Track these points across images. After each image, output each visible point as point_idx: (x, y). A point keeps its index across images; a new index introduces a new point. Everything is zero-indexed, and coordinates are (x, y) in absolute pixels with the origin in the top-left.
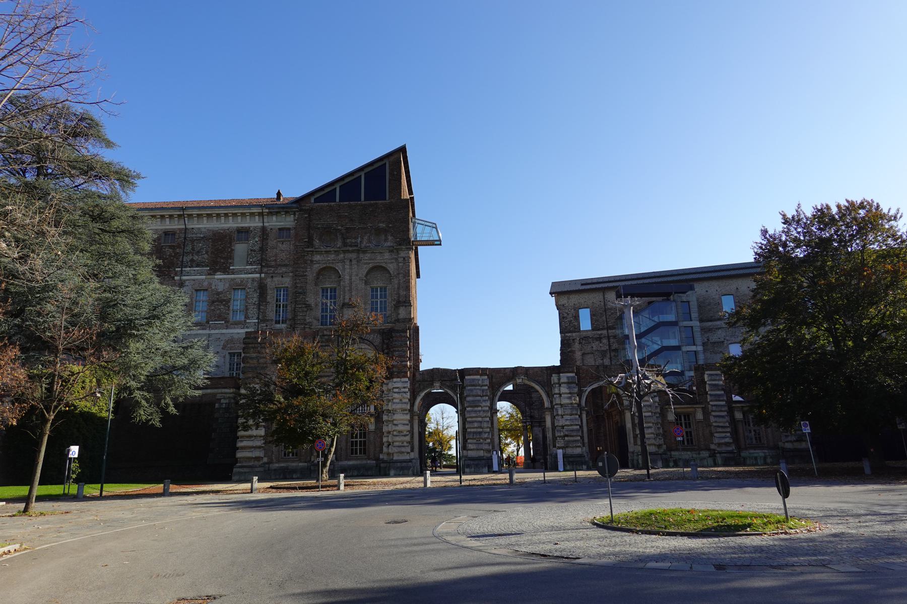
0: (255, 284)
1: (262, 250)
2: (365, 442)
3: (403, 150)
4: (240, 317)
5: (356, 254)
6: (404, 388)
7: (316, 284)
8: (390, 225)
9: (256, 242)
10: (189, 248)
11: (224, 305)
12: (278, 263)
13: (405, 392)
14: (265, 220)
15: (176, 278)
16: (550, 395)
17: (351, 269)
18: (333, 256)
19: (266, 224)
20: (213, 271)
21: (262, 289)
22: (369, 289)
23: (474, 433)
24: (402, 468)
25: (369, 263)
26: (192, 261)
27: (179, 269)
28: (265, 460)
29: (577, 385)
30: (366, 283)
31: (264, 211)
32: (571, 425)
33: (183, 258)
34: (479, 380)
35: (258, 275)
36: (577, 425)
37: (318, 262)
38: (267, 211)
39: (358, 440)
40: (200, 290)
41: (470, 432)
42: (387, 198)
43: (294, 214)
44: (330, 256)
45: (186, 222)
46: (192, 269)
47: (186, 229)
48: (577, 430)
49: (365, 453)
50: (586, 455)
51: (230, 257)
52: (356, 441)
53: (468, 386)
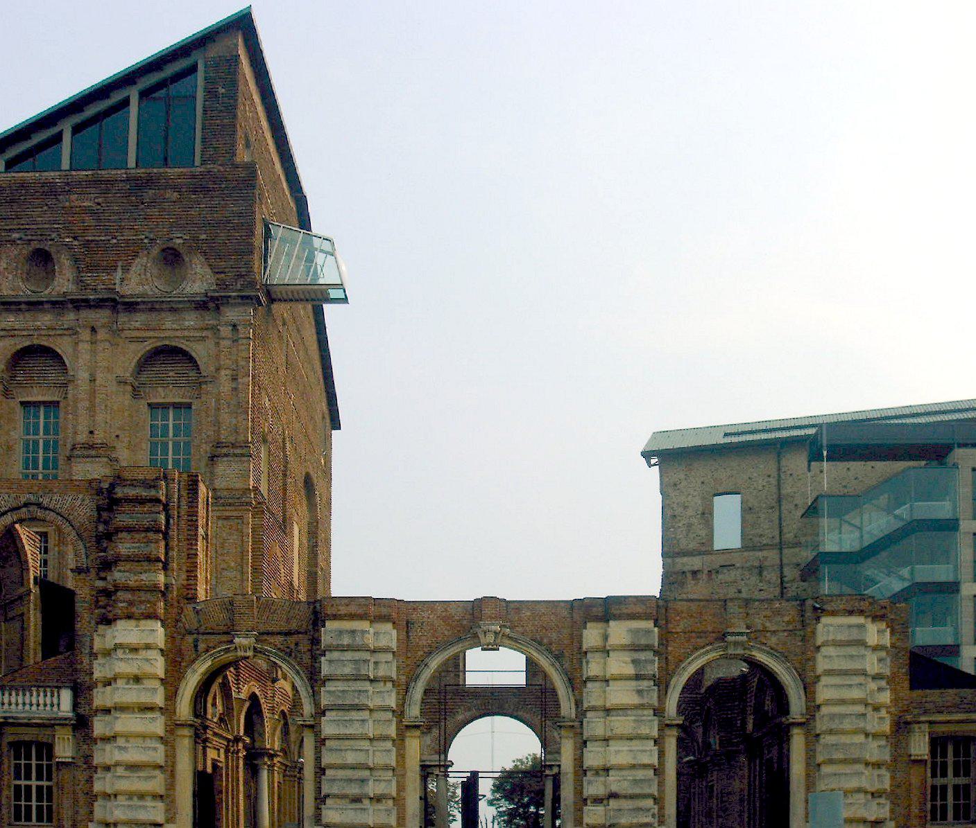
2: (49, 788)
3: (243, 25)
17: (94, 352)
25: (144, 340)
29: (656, 653)
30: (136, 394)
34: (364, 632)
36: (645, 766)
39: (34, 783)
42: (198, 161)
44: (40, 315)
49: (50, 820)
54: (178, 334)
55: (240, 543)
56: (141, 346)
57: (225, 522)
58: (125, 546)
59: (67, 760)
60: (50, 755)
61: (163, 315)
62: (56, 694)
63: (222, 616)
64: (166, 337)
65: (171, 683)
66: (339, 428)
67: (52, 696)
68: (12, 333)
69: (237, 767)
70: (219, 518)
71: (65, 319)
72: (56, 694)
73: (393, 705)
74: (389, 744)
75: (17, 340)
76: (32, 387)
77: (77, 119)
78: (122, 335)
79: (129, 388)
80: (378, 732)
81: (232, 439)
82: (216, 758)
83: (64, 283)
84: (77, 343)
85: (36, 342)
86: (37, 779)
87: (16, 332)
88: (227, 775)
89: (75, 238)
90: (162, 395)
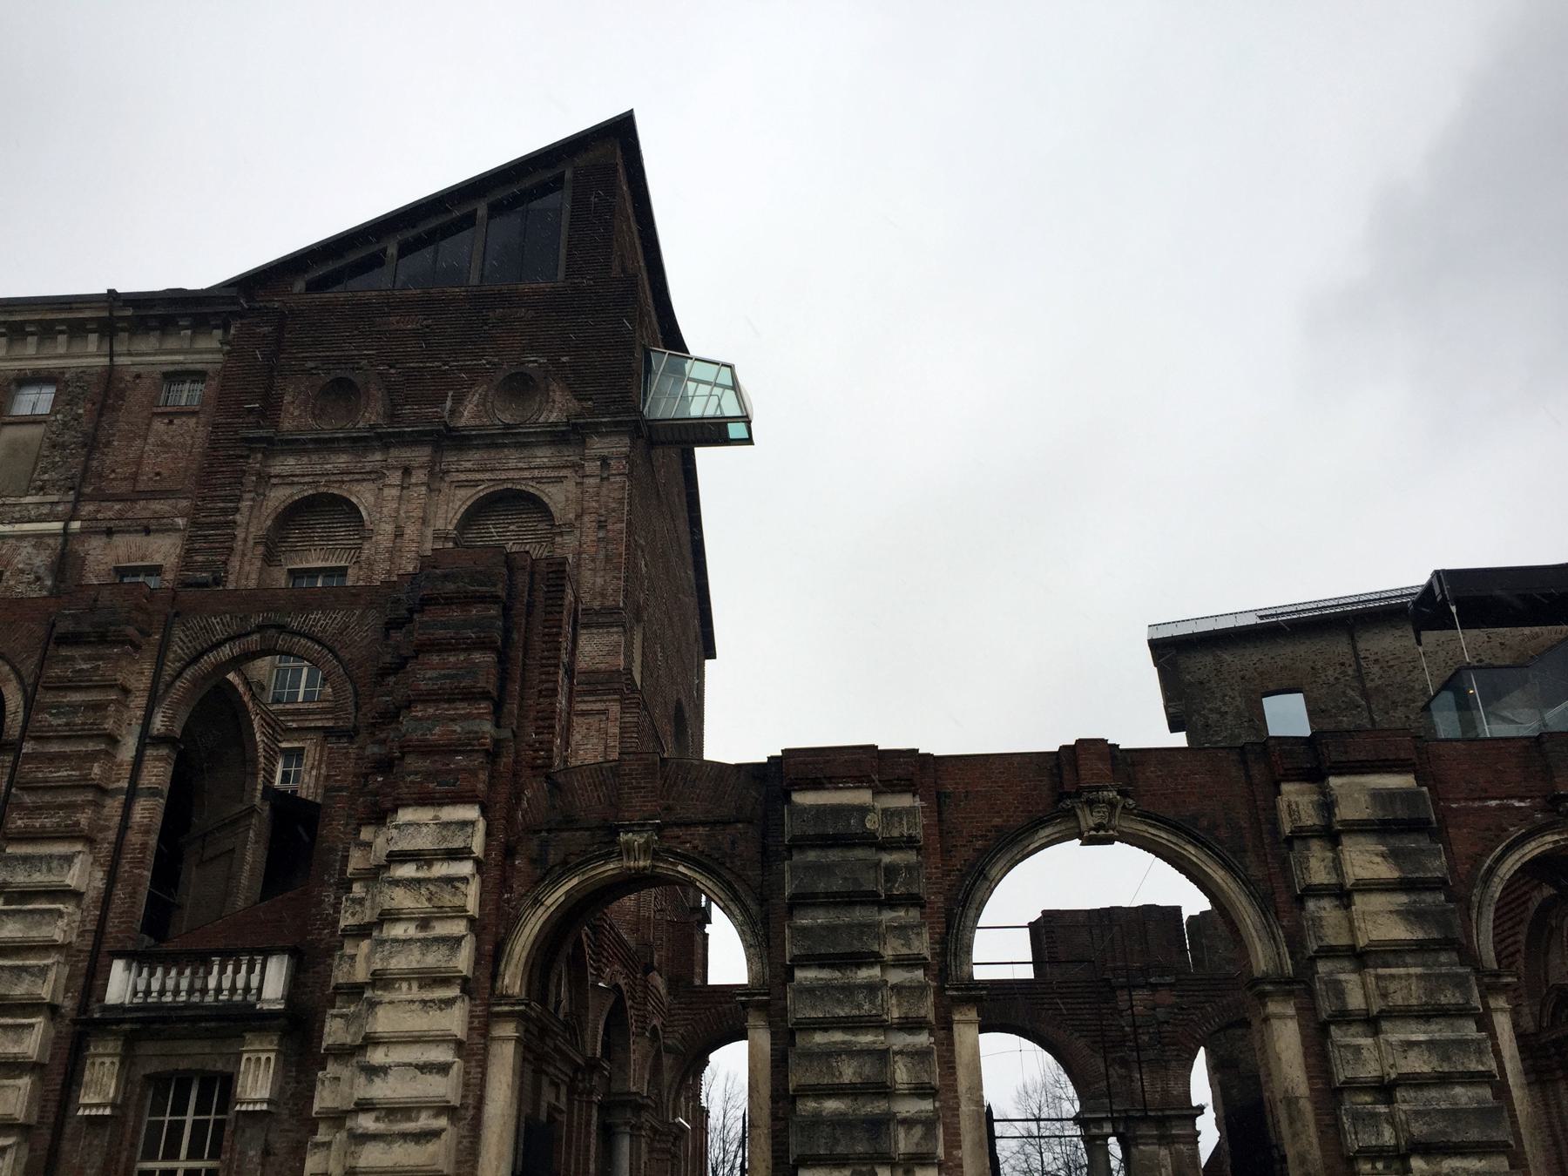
1: (92, 444)
9: (77, 418)
12: (141, 487)
13: (449, 881)
18: (344, 458)
19: (119, 360)
23: (840, 1123)
25: (476, 483)
34: (863, 810)
35: (57, 526)
37: (287, 480)
41: (817, 1120)
43: (226, 328)
44: (333, 458)
52: (194, 1153)
53: (801, 843)
54: (526, 474)
55: (601, 748)
56: (470, 492)
58: (429, 672)
59: (258, 1107)
62: (258, 967)
63: (595, 794)
64: (508, 479)
66: (712, 655)
67: (250, 971)
69: (588, 1124)
71: (368, 459)
72: (258, 967)
75: (295, 489)
76: (310, 550)
77: (410, 234)
78: (447, 479)
82: (553, 1101)
83: (371, 415)
85: (322, 490)
87: (296, 479)
88: (569, 1139)
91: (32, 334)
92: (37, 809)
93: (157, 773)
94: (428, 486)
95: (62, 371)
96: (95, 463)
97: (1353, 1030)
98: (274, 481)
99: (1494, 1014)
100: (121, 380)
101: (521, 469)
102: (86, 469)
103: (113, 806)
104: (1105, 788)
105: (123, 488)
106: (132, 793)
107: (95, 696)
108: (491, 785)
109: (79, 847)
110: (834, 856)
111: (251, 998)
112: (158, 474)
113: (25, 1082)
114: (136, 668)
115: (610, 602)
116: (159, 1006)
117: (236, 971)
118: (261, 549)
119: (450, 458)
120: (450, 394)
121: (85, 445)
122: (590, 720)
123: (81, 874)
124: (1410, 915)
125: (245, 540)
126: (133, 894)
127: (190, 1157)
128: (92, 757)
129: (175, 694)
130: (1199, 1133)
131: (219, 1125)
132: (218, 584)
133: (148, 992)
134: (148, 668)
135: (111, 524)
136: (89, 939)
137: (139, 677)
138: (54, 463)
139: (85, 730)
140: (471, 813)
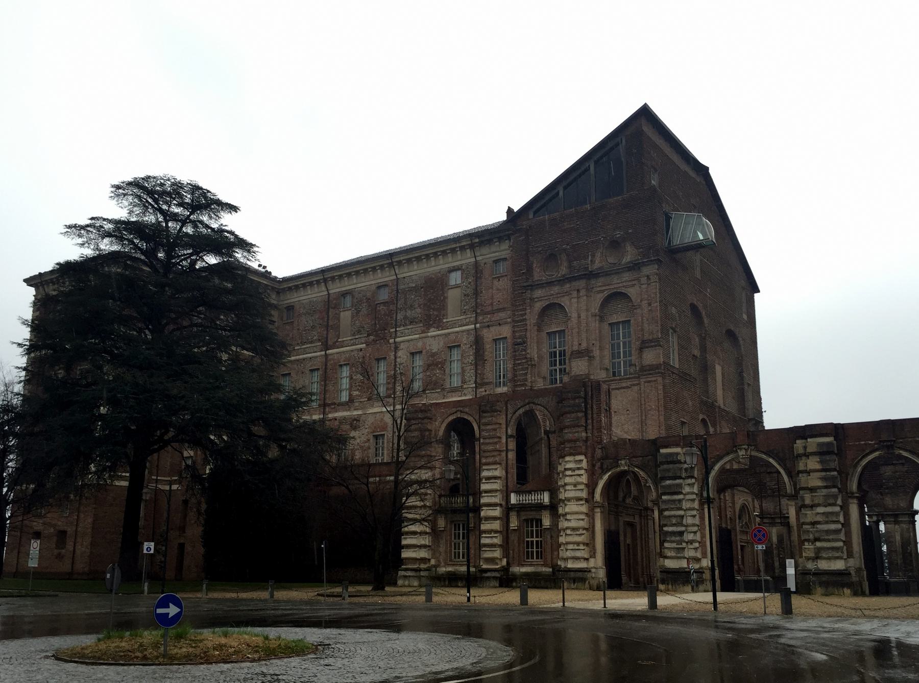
0: (472, 338)
1: (476, 293)
2: (541, 541)
4: (456, 382)
5: (584, 281)
6: (579, 469)
7: (539, 330)
8: (630, 231)
9: (470, 283)
10: (400, 303)
11: (440, 369)
12: (495, 308)
13: (579, 475)
14: (477, 254)
15: (392, 341)
16: (793, 474)
19: (478, 259)
20: (428, 327)
21: (478, 343)
22: (606, 327)
24: (574, 580)
25: (603, 291)
26: (405, 318)
27: (394, 330)
28: (433, 562)
30: (602, 319)
31: (473, 241)
32: (827, 523)
33: (396, 315)
34: (677, 454)
35: (473, 326)
37: (540, 299)
38: (477, 240)
39: (535, 539)
40: (416, 353)
45: (397, 272)
46: (406, 328)
47: (398, 279)
48: (837, 532)
50: (853, 572)
51: (443, 307)
52: (532, 542)
53: (662, 463)
54: (621, 285)
55: (656, 394)
57: (649, 384)
58: (567, 421)
60: (541, 526)
61: (613, 276)
65: (591, 487)
66: (758, 291)
67: (541, 495)
68: (540, 299)
70: (645, 382)
73: (696, 492)
74: (694, 513)
79: (598, 318)
80: (688, 506)
81: (651, 338)
83: (564, 270)
84: (571, 300)
86: (536, 537)
89: (567, 245)
90: (615, 319)
91: (449, 253)
92: (487, 457)
93: (512, 445)
94: (586, 296)
95: (462, 265)
96: (478, 300)
97: (807, 509)
98: (536, 300)
99: (851, 505)
100: (480, 266)
101: (619, 283)
102: (477, 303)
103: (504, 454)
104: (744, 445)
105: (489, 309)
106: (507, 451)
107: (494, 427)
108: (586, 449)
109: (498, 466)
110: (671, 466)
111: (542, 501)
112: (499, 301)
113: (498, 522)
114: (501, 417)
115: (655, 336)
116: (522, 504)
117: (538, 495)
118: (536, 328)
119: (593, 282)
120: (590, 253)
121: (474, 294)
122: (652, 384)
123: (498, 472)
124: (823, 479)
125: (530, 325)
126: (512, 476)
127: (536, 537)
128: (496, 443)
129: (512, 423)
130: (916, 521)
131: (541, 530)
132: (525, 343)
133: (520, 501)
134: (504, 417)
135: (489, 324)
136: (505, 488)
137: (502, 420)
138: (466, 302)
139: (493, 456)
140: (582, 457)
